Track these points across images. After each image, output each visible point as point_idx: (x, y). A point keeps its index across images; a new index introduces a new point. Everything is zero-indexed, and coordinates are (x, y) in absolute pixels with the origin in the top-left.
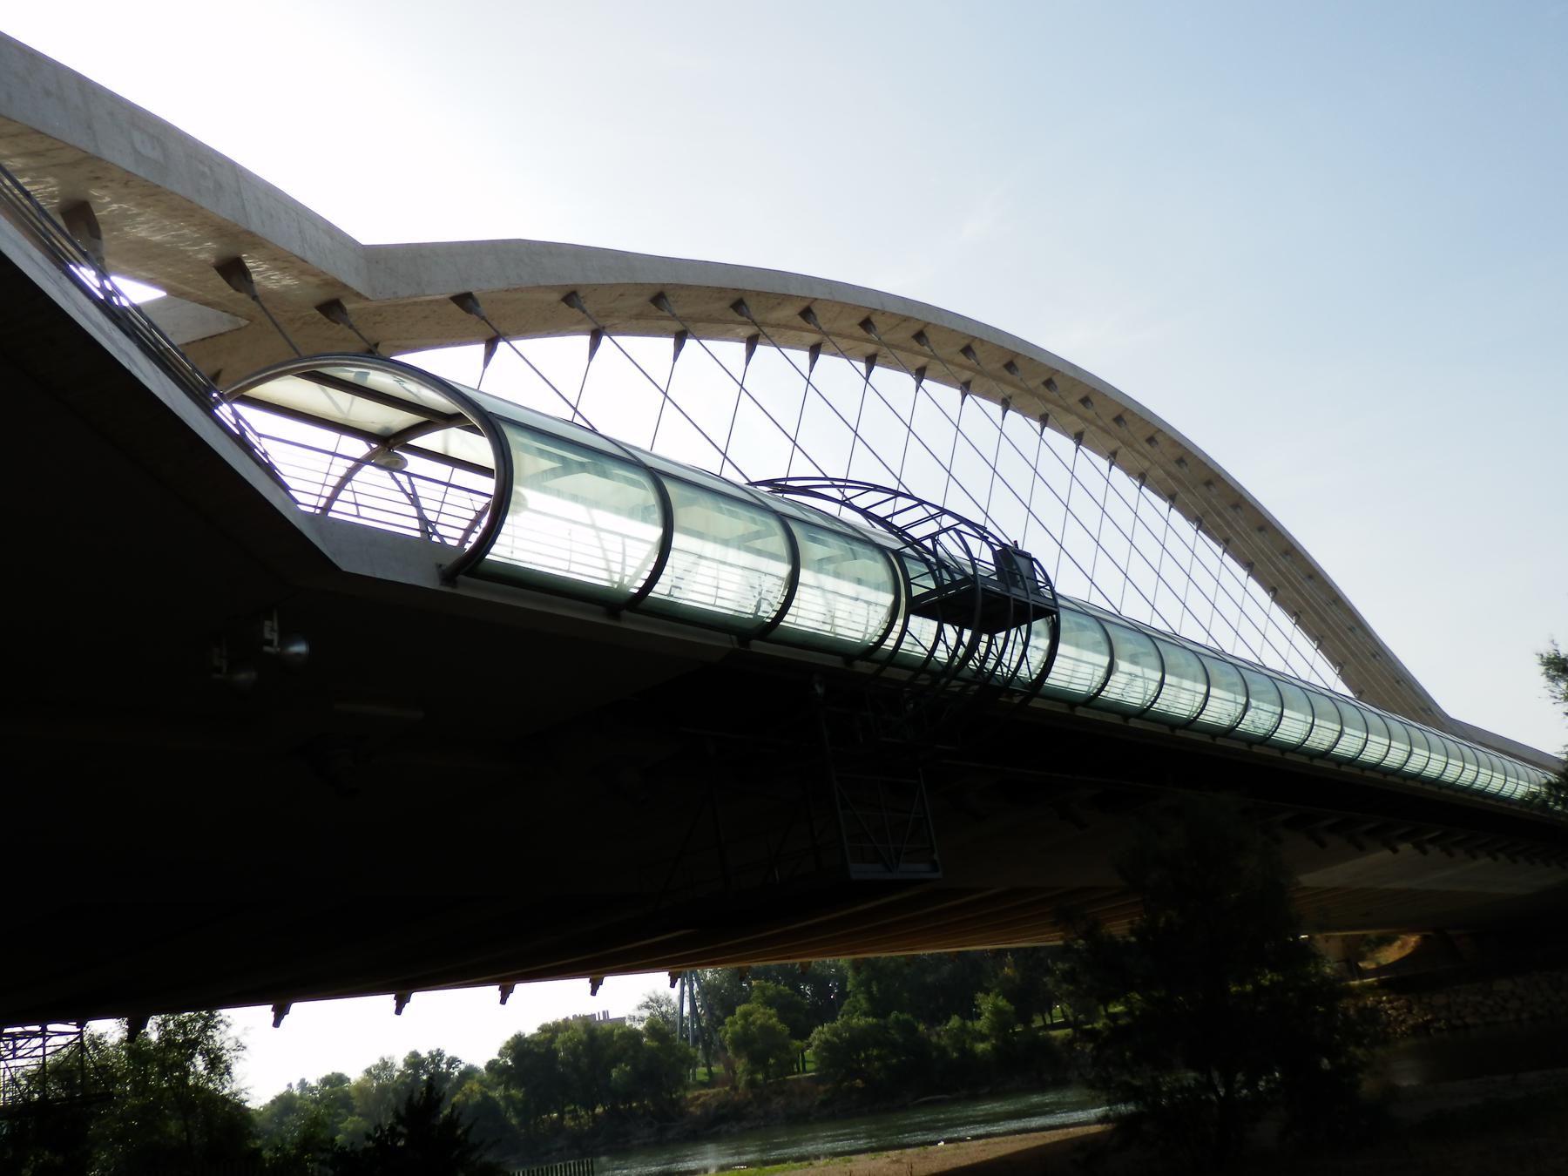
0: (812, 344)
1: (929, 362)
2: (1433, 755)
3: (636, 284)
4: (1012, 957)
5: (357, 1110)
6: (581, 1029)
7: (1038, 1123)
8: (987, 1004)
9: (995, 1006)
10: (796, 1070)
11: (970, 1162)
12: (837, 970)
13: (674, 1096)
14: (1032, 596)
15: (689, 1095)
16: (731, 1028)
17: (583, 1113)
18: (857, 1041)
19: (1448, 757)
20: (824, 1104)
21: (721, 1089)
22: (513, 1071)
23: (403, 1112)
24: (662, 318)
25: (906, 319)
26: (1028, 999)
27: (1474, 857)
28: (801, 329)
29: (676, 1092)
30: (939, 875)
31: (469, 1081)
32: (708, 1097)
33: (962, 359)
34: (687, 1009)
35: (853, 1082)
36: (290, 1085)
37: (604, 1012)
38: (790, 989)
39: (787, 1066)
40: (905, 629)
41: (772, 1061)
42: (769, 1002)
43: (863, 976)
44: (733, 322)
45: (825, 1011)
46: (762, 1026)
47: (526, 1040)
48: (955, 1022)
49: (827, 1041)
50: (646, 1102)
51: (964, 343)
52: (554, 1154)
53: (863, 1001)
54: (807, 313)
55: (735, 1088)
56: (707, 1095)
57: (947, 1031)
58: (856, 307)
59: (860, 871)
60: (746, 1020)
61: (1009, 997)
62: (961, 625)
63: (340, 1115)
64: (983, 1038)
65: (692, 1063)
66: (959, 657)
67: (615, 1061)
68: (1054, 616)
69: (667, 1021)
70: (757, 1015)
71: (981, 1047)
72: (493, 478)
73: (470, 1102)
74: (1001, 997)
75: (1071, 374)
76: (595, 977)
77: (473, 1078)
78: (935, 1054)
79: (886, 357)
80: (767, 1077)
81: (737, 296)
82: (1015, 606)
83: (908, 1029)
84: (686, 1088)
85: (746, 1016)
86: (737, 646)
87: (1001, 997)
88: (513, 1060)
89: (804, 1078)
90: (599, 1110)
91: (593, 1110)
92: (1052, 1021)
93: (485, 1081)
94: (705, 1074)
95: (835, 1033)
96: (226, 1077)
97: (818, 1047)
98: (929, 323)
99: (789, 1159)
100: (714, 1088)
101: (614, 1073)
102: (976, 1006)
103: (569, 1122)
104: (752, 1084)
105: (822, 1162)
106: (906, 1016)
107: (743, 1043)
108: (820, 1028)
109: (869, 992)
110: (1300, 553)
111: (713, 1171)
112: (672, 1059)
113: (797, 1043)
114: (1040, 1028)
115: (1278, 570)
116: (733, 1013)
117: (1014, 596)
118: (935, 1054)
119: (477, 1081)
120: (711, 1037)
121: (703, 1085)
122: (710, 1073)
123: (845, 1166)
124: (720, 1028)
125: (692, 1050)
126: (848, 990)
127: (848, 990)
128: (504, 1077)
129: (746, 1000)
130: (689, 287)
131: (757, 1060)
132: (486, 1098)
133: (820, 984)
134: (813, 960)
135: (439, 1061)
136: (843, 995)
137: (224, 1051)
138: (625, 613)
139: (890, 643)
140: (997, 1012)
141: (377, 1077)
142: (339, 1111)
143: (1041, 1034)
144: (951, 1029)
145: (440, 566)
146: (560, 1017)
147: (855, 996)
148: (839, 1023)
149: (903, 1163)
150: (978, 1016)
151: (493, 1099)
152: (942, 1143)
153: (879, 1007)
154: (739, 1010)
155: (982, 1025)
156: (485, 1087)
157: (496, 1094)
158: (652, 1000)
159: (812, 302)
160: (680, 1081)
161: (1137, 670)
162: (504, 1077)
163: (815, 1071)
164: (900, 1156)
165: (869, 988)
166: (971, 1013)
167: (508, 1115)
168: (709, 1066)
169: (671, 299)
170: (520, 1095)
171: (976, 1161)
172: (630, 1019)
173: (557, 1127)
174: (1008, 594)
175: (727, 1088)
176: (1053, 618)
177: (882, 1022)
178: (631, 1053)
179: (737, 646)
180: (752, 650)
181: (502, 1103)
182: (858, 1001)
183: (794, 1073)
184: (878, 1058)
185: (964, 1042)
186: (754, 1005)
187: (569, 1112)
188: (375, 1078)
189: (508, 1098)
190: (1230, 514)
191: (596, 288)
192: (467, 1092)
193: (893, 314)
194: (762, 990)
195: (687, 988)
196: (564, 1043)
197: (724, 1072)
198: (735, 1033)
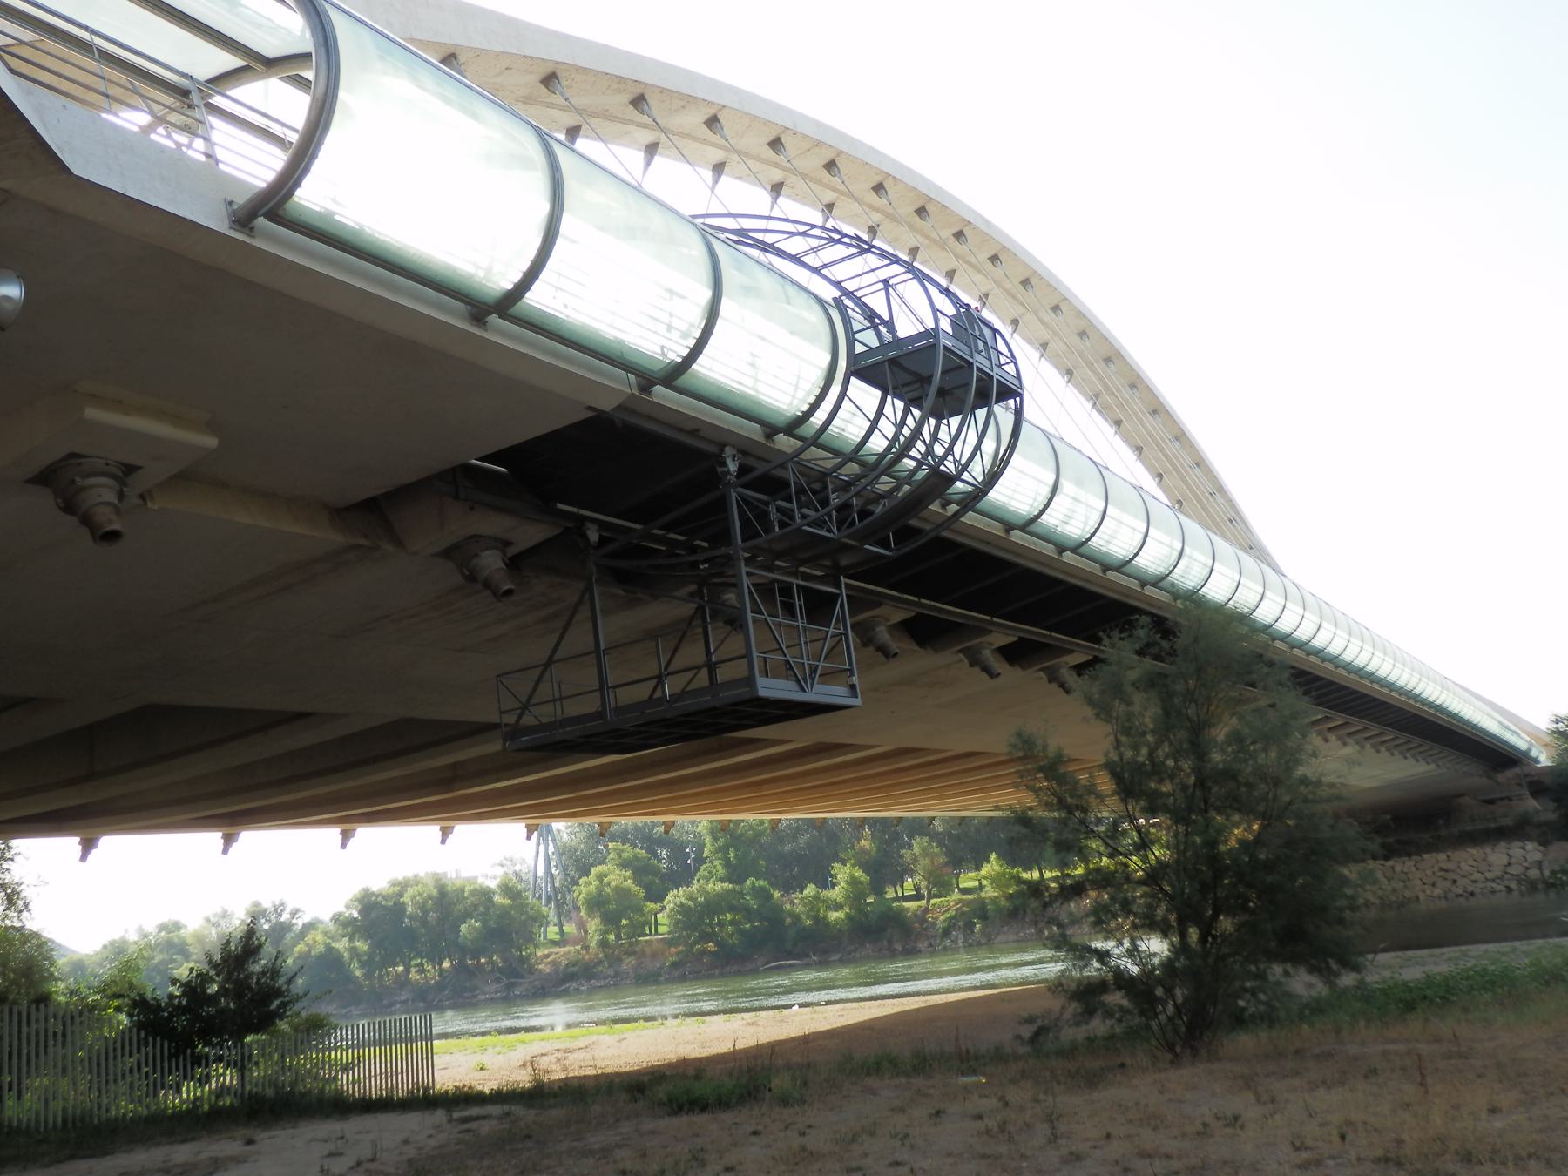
0: (715, 163)
1: (838, 197)
2: (1338, 632)
3: (526, 57)
4: (870, 830)
5: (194, 957)
6: (431, 884)
7: (891, 989)
8: (843, 873)
9: (851, 875)
10: (648, 932)
11: (829, 1027)
12: (695, 836)
13: (524, 953)
14: (996, 369)
15: (540, 953)
16: (586, 888)
17: (430, 967)
18: (713, 906)
19: (1350, 635)
20: (675, 965)
21: (572, 948)
22: (359, 924)
23: (217, 957)
24: (551, 106)
25: (819, 144)
26: (884, 870)
27: (1345, 744)
28: (704, 141)
29: (527, 948)
30: (857, 702)
31: (312, 932)
32: (557, 956)
33: (872, 197)
34: (541, 872)
35: (706, 946)
36: (126, 931)
37: (456, 871)
38: (647, 852)
39: (638, 928)
40: (843, 394)
41: (624, 922)
42: (625, 865)
43: (721, 842)
44: (631, 122)
45: (681, 877)
46: (616, 887)
47: (373, 894)
48: (810, 890)
49: (682, 905)
50: (494, 958)
51: (877, 179)
52: (398, 1006)
53: (719, 868)
54: (713, 122)
55: (586, 948)
56: (557, 953)
57: (802, 899)
58: (767, 123)
59: (772, 688)
60: (601, 881)
61: (865, 867)
62: (911, 402)
63: (174, 961)
64: (838, 907)
65: (542, 920)
66: (904, 436)
67: (464, 917)
68: (1018, 399)
69: (521, 881)
70: (611, 877)
71: (834, 916)
72: (309, 94)
73: (313, 953)
74: (857, 868)
75: (983, 228)
76: (446, 824)
77: (316, 929)
78: (788, 920)
79: (793, 187)
80: (618, 937)
81: (638, 90)
82: (979, 380)
83: (763, 895)
84: (536, 946)
85: (601, 877)
86: (636, 392)
87: (857, 868)
88: (360, 912)
89: (657, 940)
90: (446, 964)
91: (440, 964)
92: (903, 893)
93: (330, 931)
94: (557, 934)
95: (691, 897)
96: (25, 914)
97: (672, 910)
98: (842, 152)
99: (640, 1018)
100: (564, 946)
101: (463, 929)
102: (832, 876)
103: (414, 975)
104: (603, 944)
105: (671, 1022)
106: (762, 883)
107: (597, 903)
108: (675, 891)
109: (727, 860)
110: (1190, 441)
111: (559, 1029)
112: (523, 917)
113: (651, 905)
114: (893, 900)
115: (1166, 456)
116: (587, 873)
117: (978, 365)
118: (788, 920)
119: (321, 932)
120: (564, 897)
121: (554, 943)
122: (562, 932)
123: (699, 1027)
124: (575, 887)
125: (545, 909)
126: (705, 855)
127: (705, 855)
128: (349, 930)
129: (603, 862)
130: (585, 70)
131: (611, 920)
132: (329, 949)
133: (678, 850)
134: (680, 819)
135: (282, 911)
136: (700, 860)
137: (22, 887)
138: (493, 319)
139: (819, 417)
140: (853, 882)
141: (216, 925)
142: (174, 957)
143: (894, 905)
144: (807, 898)
145: (231, 203)
146: (410, 874)
147: (711, 862)
148: (695, 887)
149: (759, 1026)
150: (834, 886)
151: (337, 950)
152: (797, 1007)
153: (735, 874)
154: (594, 871)
155: (836, 894)
156: (328, 938)
157: (342, 945)
158: (506, 859)
159: (720, 110)
160: (530, 939)
161: (1082, 495)
162: (349, 930)
163: (669, 933)
164: (754, 1019)
165: (726, 853)
166: (825, 882)
167: (352, 966)
168: (561, 926)
169: (564, 82)
170: (366, 948)
171: (835, 1026)
172: (482, 876)
173: (402, 982)
174: (971, 360)
175: (578, 947)
176: (1016, 402)
177: (737, 888)
178: (482, 909)
179: (636, 392)
180: (655, 400)
181: (346, 955)
182: (715, 867)
183: (647, 935)
184: (732, 923)
185: (818, 911)
186: (610, 866)
187: (416, 965)
188: (213, 925)
189: (354, 951)
190: (1127, 393)
191: (479, 53)
192: (311, 942)
193: (805, 136)
194: (619, 853)
195: (542, 848)
196: (413, 898)
197: (575, 931)
198: (589, 894)
